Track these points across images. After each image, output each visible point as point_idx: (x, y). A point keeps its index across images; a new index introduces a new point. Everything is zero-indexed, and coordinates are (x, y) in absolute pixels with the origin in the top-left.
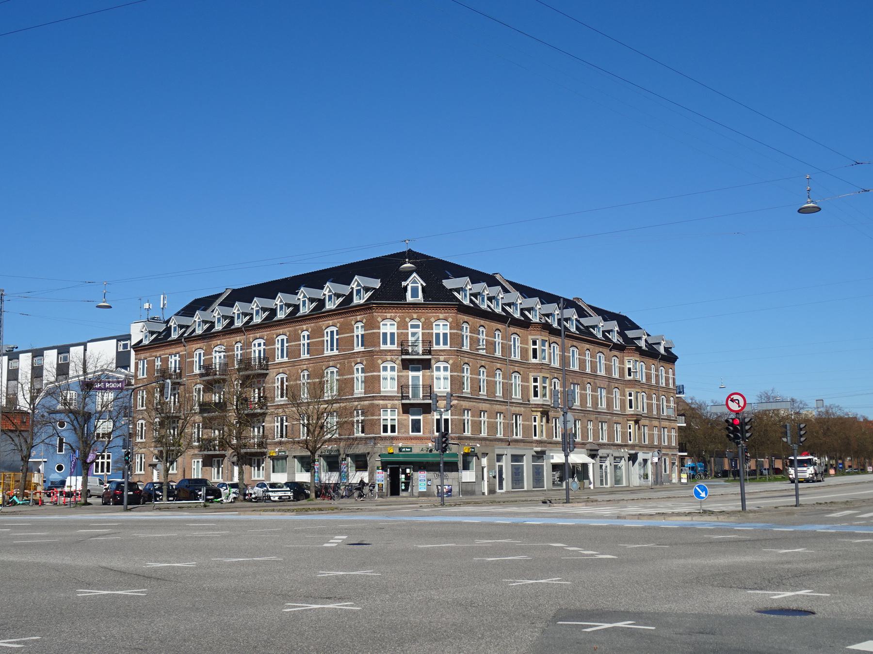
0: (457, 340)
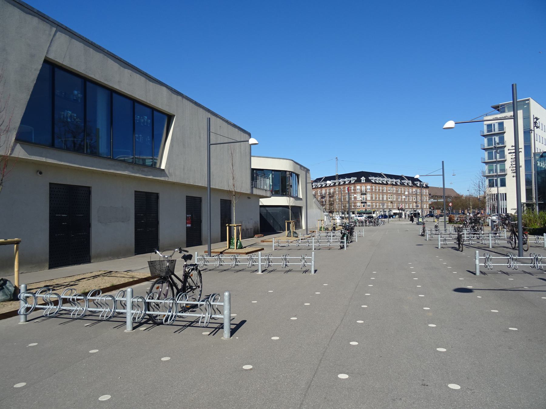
0: (372, 189)
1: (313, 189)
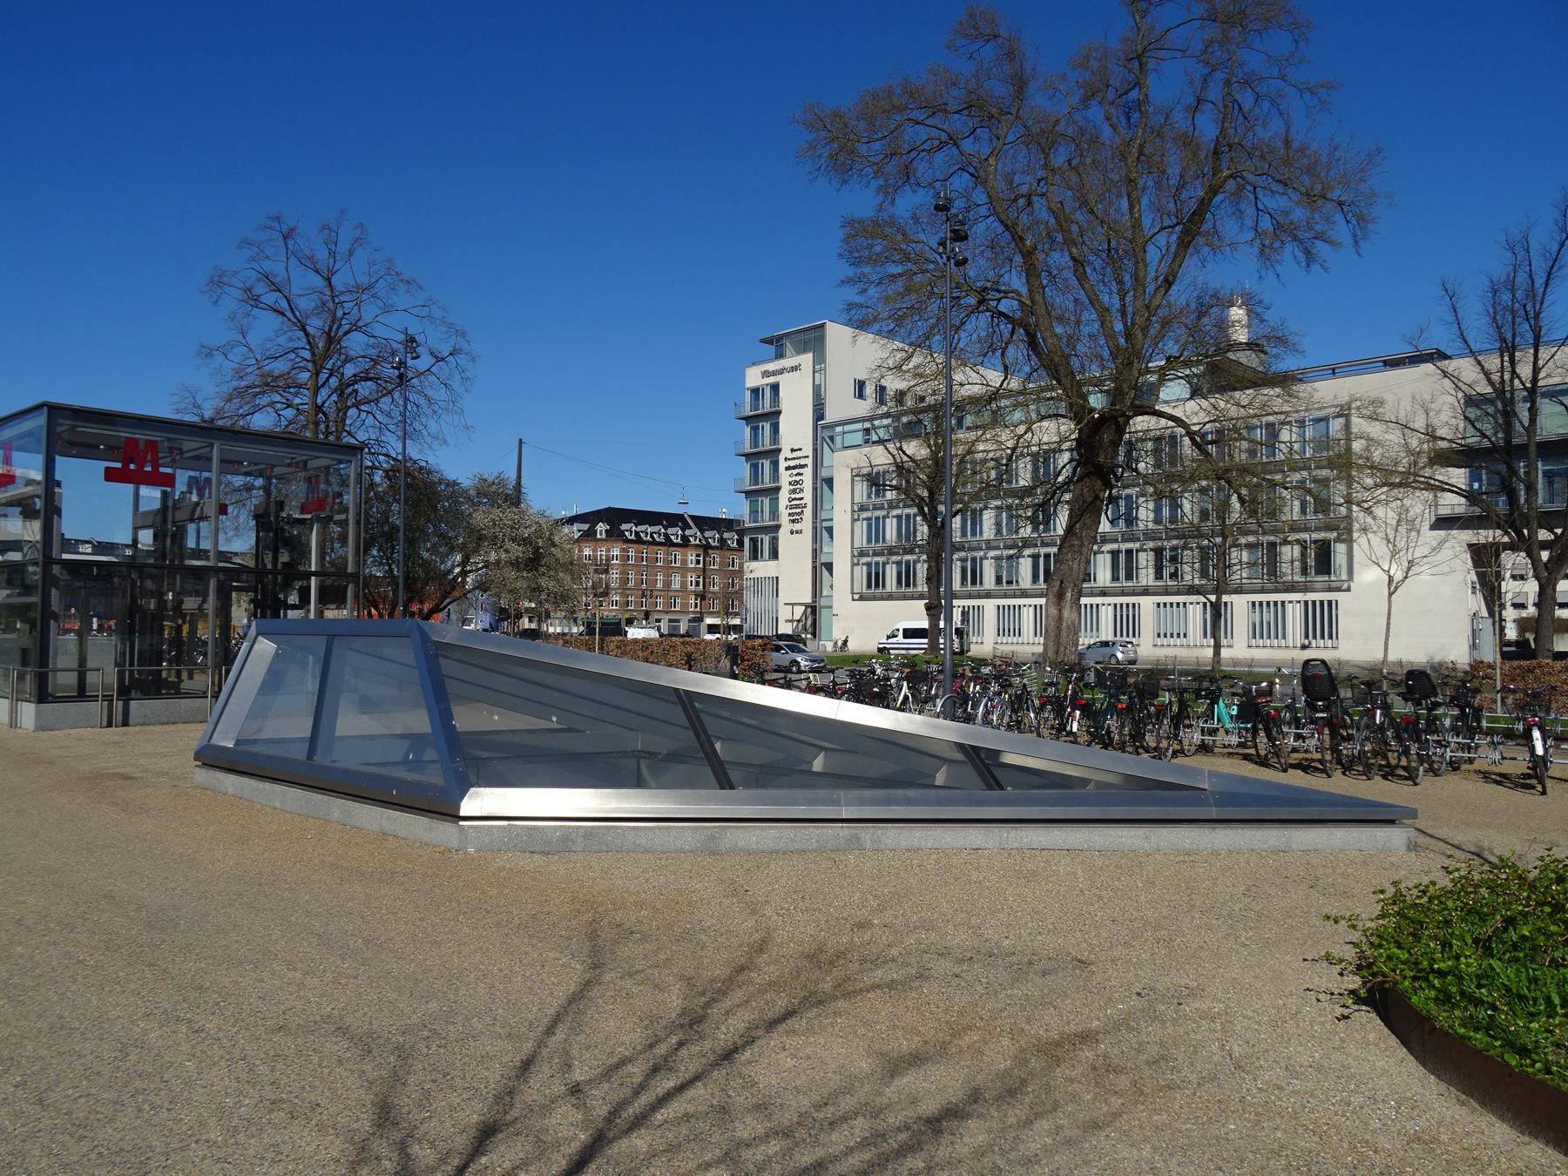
1: (853, 600)
